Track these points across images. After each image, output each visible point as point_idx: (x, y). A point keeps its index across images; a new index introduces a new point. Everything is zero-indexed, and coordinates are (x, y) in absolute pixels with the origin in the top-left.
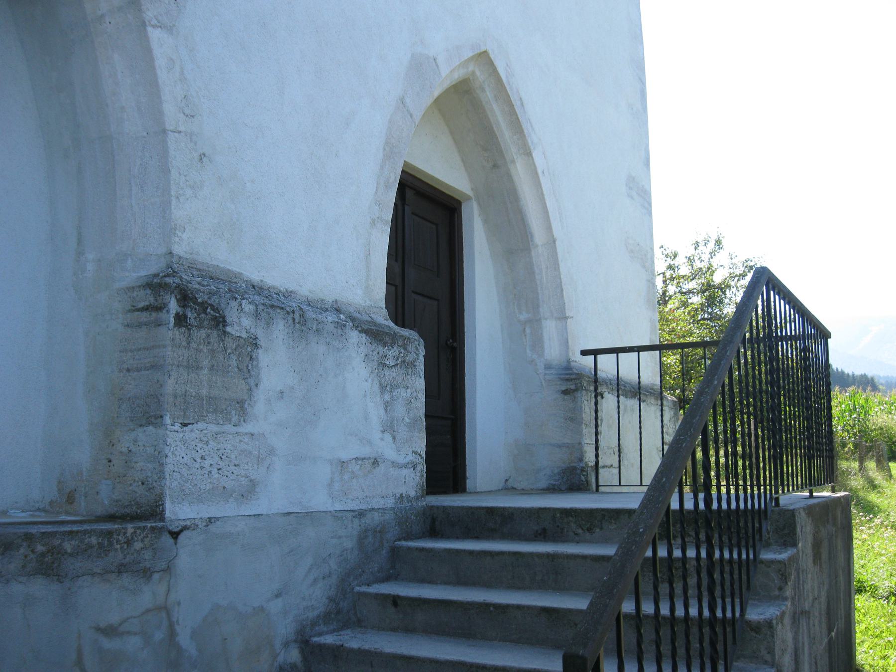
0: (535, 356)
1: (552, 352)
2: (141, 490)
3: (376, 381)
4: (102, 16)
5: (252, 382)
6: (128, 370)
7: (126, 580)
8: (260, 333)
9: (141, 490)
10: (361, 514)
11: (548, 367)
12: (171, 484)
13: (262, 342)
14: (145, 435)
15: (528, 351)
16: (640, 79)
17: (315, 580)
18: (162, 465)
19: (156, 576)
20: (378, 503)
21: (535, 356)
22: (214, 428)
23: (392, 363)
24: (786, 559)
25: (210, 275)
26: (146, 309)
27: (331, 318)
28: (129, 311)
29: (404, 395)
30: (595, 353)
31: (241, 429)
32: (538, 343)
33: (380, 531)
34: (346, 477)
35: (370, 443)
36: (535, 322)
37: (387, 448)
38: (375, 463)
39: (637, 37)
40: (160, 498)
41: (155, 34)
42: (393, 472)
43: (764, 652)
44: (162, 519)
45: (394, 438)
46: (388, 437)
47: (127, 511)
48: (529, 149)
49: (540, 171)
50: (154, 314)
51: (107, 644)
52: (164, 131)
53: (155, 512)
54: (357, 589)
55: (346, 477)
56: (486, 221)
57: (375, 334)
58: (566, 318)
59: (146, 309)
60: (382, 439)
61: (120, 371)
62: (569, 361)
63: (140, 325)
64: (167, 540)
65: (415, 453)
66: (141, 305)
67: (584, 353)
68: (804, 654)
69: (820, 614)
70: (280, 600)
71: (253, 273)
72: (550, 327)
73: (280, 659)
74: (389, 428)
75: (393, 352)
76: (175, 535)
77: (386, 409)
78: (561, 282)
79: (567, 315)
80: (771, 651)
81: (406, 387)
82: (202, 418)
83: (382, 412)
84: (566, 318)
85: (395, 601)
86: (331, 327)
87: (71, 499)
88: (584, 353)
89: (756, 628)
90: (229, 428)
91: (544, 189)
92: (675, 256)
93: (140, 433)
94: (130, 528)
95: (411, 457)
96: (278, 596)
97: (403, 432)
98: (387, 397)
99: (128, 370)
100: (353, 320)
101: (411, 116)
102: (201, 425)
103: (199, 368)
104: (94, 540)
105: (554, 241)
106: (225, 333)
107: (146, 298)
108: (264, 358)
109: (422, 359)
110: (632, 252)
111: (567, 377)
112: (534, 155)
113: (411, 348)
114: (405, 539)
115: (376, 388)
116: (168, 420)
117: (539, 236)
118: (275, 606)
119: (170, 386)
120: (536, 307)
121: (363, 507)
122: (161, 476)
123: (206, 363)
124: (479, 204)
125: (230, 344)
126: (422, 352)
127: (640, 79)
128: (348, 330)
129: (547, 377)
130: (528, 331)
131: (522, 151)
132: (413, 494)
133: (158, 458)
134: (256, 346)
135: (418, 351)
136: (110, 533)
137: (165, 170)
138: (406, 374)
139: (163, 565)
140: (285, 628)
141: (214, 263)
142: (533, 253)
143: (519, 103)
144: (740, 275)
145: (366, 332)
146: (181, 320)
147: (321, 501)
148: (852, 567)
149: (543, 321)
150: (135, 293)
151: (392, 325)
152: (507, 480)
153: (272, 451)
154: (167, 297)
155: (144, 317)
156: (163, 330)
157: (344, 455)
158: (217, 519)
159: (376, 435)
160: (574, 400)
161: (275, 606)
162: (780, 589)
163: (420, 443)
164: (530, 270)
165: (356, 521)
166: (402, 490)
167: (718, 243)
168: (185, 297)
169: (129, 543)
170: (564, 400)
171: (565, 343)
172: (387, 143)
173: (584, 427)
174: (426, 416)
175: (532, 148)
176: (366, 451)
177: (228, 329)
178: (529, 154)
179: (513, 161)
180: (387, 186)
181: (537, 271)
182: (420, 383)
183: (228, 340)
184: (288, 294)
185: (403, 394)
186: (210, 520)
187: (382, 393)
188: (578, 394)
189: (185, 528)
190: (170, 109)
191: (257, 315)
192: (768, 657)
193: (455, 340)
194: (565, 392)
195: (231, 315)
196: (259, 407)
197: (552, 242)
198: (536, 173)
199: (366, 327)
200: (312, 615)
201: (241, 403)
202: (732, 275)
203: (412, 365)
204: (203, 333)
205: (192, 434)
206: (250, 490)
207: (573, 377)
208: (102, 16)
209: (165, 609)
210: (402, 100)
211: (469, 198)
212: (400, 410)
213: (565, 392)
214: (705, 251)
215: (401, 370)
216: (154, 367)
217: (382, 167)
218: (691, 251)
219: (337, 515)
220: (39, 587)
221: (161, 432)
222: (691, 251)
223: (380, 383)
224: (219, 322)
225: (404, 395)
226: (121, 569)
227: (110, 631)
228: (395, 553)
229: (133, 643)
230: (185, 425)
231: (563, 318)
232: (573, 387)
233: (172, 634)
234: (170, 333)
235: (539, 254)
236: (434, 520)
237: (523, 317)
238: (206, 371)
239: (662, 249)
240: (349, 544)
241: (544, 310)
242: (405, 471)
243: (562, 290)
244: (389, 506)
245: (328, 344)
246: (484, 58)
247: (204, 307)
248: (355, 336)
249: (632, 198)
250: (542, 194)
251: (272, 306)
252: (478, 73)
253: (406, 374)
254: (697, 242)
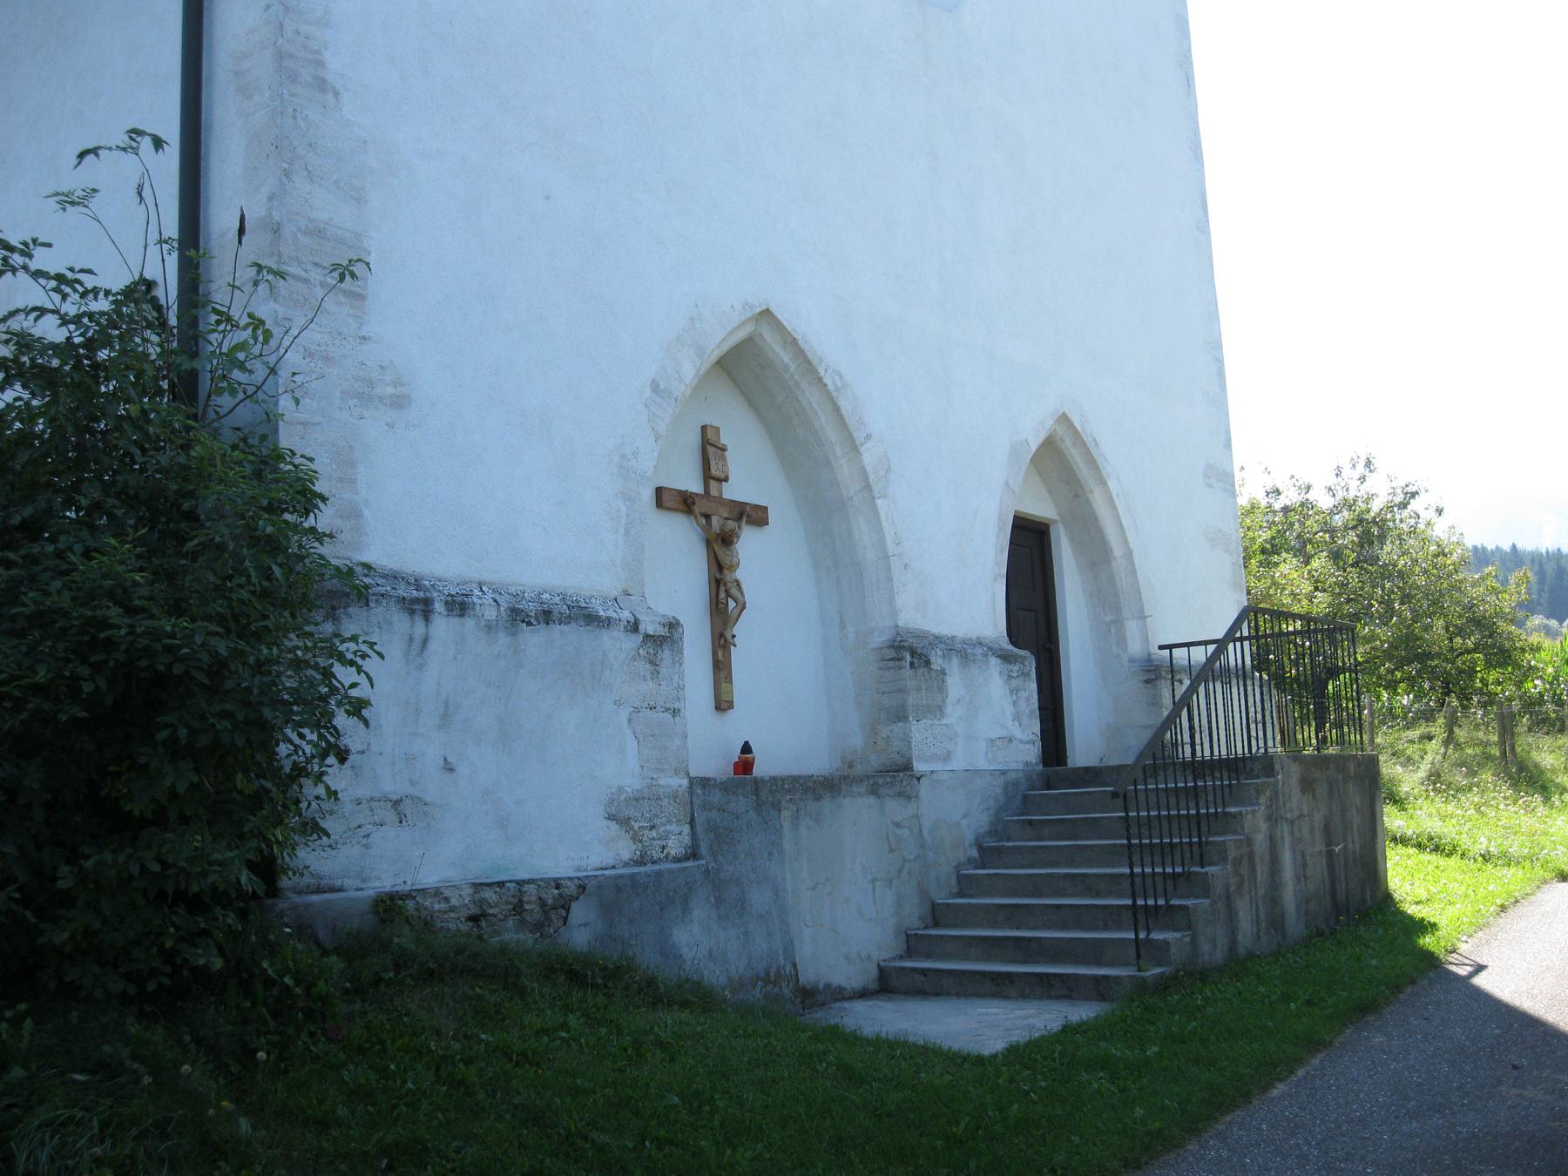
0: (1120, 652)
1: (1135, 647)
2: (898, 757)
3: (1007, 688)
4: (852, 497)
5: (945, 695)
6: (883, 693)
7: (902, 800)
8: (946, 667)
9: (898, 757)
10: (1004, 772)
11: (1132, 660)
12: (915, 752)
13: (947, 671)
14: (897, 728)
15: (1114, 647)
16: (1217, 359)
17: (983, 811)
18: (909, 742)
19: (913, 799)
20: (1013, 766)
21: (1120, 652)
22: (930, 722)
23: (1015, 675)
24: (139, 414)
25: (921, 635)
26: (891, 660)
27: (979, 651)
28: (880, 661)
29: (1024, 695)
30: (1170, 647)
31: (942, 722)
32: (1122, 640)
33: (1016, 784)
34: (995, 749)
35: (1006, 728)
36: (1119, 622)
37: (1017, 732)
38: (1010, 741)
39: (1212, 316)
40: (910, 759)
41: (879, 502)
42: (1021, 746)
43: (1239, 829)
44: (913, 771)
45: (1020, 724)
46: (1017, 724)
47: (889, 768)
48: (1104, 480)
49: (1114, 496)
50: (897, 663)
51: (898, 831)
52: (888, 556)
53: (907, 767)
54: (1006, 818)
55: (995, 749)
56: (1071, 539)
57: (1005, 658)
58: (1145, 617)
59: (891, 660)
60: (1013, 725)
61: (878, 693)
62: (1149, 654)
63: (888, 669)
64: (915, 781)
65: (1033, 733)
66: (888, 657)
67: (1161, 647)
68: (1283, 843)
69: (1312, 832)
70: (966, 819)
71: (935, 629)
72: (1131, 626)
73: (969, 853)
74: (1017, 717)
75: (1015, 668)
76: (919, 779)
77: (1014, 706)
78: (1139, 586)
79: (1147, 615)
80: (1243, 828)
81: (1025, 690)
82: (924, 717)
83: (1012, 709)
84: (1145, 617)
85: (1030, 823)
86: (980, 657)
87: (851, 765)
88: (1161, 647)
89: (1234, 816)
90: (936, 721)
91: (1119, 510)
92: (1309, 488)
93: (894, 727)
94: (901, 774)
95: (1031, 736)
96: (965, 817)
97: (1025, 720)
98: (1014, 697)
99: (883, 693)
100: (991, 649)
101: (1014, 492)
102: (924, 721)
103: (921, 690)
104: (889, 779)
105: (1131, 553)
106: (931, 669)
107: (891, 654)
108: (949, 680)
109: (1034, 669)
110: (1213, 539)
111: (1148, 668)
112: (1109, 484)
113: (1026, 663)
114: (1031, 790)
115: (1008, 692)
116: (911, 719)
117: (1117, 550)
118: (964, 822)
119: (910, 701)
120: (1117, 609)
121: (1006, 768)
122: (910, 748)
123: (924, 687)
124: (1066, 527)
125: (933, 674)
126: (1034, 666)
127: (1217, 359)
128: (989, 657)
129: (1131, 669)
130: (1113, 630)
131: (1098, 482)
132: (1034, 761)
133: (907, 739)
134: (945, 674)
135: (1031, 665)
136: (894, 776)
137: (890, 579)
138: (1025, 681)
139: (915, 795)
140: (969, 837)
141: (916, 627)
142: (1113, 565)
143: (1093, 444)
144: (1401, 503)
145: (999, 657)
146: (912, 664)
147: (982, 764)
148: (1378, 816)
149: (1125, 622)
150: (883, 651)
151: (1011, 647)
152: (1102, 759)
153: (956, 734)
154: (905, 653)
155: (891, 664)
156: (902, 671)
157: (994, 736)
158: (935, 771)
159: (1010, 723)
160: (1155, 687)
161: (964, 822)
162: (1257, 799)
163: (1037, 728)
164: (1112, 579)
165: (1002, 776)
166: (1028, 758)
167: (1368, 463)
168: (913, 653)
169: (901, 782)
170: (1146, 688)
171: (1146, 639)
172: (999, 520)
173: (1164, 709)
174: (1039, 708)
175: (1106, 477)
176: (1004, 733)
177: (932, 667)
178: (1105, 484)
179: (1091, 492)
180: (1002, 550)
181: (1117, 580)
182: (1034, 686)
183: (932, 673)
184: (953, 638)
185: (1024, 695)
186: (932, 772)
187: (1011, 695)
188: (1158, 683)
189: (922, 776)
190: (889, 543)
191: (944, 656)
192: (1242, 832)
193: (1051, 643)
194: (1147, 682)
195: (933, 659)
196: (949, 709)
197: (1129, 554)
198: (1111, 498)
199: (999, 653)
200: (982, 831)
201: (940, 707)
202: (1389, 505)
203: (1027, 675)
204: (922, 670)
205: (921, 725)
206: (947, 757)
207: (1153, 668)
208: (852, 497)
209: (917, 816)
210: (1007, 484)
211: (1056, 522)
212: (1023, 706)
213: (1147, 682)
214: (1350, 475)
215: (1021, 679)
216: (900, 691)
217: (998, 538)
218: (1332, 480)
219: (992, 772)
220: (872, 800)
221: (908, 725)
222: (1332, 480)
223: (1010, 688)
224: (928, 663)
225: (1024, 695)
226: (900, 794)
227: (897, 825)
228: (1026, 798)
229: (905, 832)
230: (918, 721)
231: (1142, 617)
232: (1153, 677)
233: (921, 830)
234: (908, 672)
235: (1119, 566)
236: (1049, 778)
237: (1109, 618)
238: (924, 691)
239: (1294, 480)
240: (999, 791)
241: (1126, 612)
242: (1028, 746)
243: (1140, 594)
244: (1021, 768)
245: (980, 667)
246: (1064, 419)
247: (920, 655)
248: (994, 661)
249: (1211, 486)
250: (1118, 514)
251: (951, 650)
252: (1058, 429)
253: (1025, 681)
254: (1338, 467)
